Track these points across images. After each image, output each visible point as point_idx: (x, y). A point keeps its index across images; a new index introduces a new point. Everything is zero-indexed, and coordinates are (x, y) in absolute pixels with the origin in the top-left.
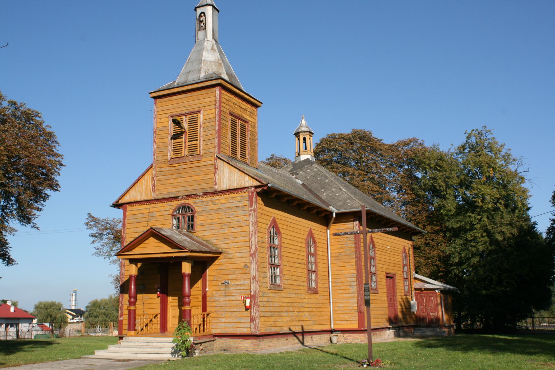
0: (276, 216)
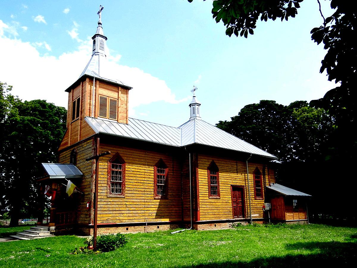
0: (119, 152)
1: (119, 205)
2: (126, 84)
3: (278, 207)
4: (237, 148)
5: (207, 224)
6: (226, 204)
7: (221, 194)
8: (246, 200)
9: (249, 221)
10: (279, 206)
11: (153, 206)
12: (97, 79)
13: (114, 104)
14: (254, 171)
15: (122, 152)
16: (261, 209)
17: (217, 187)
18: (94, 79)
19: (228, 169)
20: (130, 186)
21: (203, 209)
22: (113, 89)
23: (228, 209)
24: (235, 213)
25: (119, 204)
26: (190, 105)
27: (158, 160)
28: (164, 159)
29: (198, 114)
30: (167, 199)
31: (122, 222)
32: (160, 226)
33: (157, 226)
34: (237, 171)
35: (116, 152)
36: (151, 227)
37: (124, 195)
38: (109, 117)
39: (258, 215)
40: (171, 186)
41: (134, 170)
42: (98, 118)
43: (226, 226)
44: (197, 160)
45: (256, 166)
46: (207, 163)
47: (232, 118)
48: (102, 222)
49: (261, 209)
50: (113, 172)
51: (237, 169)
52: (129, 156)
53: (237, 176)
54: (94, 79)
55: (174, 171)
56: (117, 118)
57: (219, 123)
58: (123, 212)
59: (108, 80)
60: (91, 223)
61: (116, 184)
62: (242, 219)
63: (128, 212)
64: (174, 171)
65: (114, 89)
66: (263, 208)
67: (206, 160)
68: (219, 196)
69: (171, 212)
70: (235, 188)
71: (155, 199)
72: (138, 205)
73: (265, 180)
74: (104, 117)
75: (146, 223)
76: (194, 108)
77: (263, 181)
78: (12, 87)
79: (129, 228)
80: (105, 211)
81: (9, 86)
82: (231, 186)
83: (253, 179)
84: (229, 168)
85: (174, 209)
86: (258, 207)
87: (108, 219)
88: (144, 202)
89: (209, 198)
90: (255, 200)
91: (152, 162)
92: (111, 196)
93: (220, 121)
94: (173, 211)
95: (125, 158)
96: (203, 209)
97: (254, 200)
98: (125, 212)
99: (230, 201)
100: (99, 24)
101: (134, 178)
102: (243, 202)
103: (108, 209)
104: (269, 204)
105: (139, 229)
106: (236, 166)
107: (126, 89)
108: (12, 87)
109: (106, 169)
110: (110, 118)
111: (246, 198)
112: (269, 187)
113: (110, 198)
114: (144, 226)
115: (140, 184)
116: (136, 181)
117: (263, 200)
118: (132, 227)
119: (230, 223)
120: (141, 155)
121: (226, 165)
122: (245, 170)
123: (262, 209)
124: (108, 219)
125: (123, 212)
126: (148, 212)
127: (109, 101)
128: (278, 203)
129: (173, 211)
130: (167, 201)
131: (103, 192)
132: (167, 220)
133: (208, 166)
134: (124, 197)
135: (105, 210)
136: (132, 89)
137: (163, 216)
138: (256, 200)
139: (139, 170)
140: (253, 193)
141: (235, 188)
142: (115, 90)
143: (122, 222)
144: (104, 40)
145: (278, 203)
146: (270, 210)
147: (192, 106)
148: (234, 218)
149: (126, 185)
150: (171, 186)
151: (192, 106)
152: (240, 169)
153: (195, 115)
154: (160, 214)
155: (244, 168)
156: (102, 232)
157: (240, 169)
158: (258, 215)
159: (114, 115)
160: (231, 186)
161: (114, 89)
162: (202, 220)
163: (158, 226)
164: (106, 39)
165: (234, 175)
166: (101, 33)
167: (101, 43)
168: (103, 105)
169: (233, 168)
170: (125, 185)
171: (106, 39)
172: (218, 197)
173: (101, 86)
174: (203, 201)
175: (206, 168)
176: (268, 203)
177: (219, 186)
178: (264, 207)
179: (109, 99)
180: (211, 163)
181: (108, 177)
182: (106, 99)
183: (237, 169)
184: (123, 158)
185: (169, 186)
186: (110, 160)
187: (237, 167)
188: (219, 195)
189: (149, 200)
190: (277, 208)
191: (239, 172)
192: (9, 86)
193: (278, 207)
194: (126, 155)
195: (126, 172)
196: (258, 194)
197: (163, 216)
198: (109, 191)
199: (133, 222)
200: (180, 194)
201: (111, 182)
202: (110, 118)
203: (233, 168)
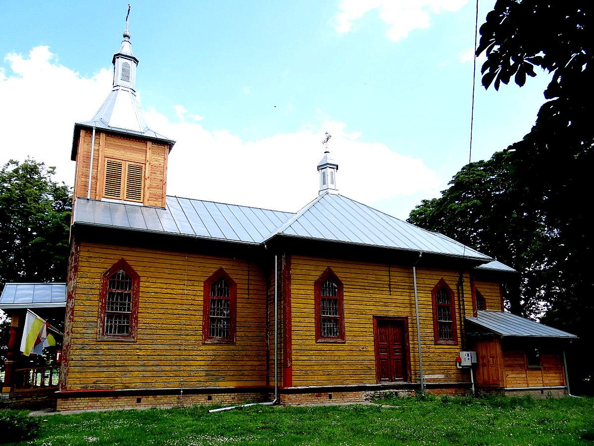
0: (126, 258)
1: (123, 356)
2: (162, 135)
3: (491, 359)
4: (428, 244)
5: (310, 394)
6: (359, 353)
7: (347, 334)
8: (411, 346)
9: (417, 388)
10: (493, 357)
11: (199, 358)
12: (99, 131)
13: (136, 173)
14: (434, 286)
15: (341, 271)
16: (452, 363)
17: (339, 322)
18: (94, 131)
19: (367, 284)
20: (148, 321)
21: (300, 363)
22: (135, 146)
23: (366, 363)
24: (383, 370)
25: (123, 354)
26: (320, 167)
27: (215, 270)
28: (226, 269)
29: (332, 183)
30: (234, 344)
31: (127, 387)
32: (214, 396)
33: (136, 397)
34: (390, 288)
35: (120, 257)
36: (193, 398)
37: (133, 337)
38: (126, 197)
39: (441, 376)
40: (243, 320)
41: (158, 290)
42: (103, 199)
43: (361, 399)
44: (288, 267)
45: (218, 266)
46: (314, 273)
47: (443, 192)
48: (84, 387)
49: (452, 363)
50: (112, 295)
51: (390, 285)
52: (149, 265)
53: (390, 297)
54: (94, 131)
55: (251, 292)
56: (142, 199)
57: (422, 204)
58: (131, 369)
59: (140, 134)
60: (60, 389)
61: (119, 316)
62: (401, 383)
63: (141, 369)
64: (251, 292)
65: (137, 147)
66: (456, 362)
67: (312, 268)
68: (343, 339)
69: (240, 368)
70: (381, 322)
71: (204, 344)
72: (164, 355)
73: (464, 305)
74: (116, 198)
75: (180, 390)
76: (324, 173)
77: (457, 307)
78: (54, 168)
79: (144, 399)
80: (90, 366)
81: (51, 168)
82: (375, 317)
83: (431, 303)
84: (370, 281)
85: (250, 363)
86: (444, 359)
87: (98, 381)
88: (180, 350)
89: (316, 343)
90: (435, 345)
91: (199, 274)
92: (105, 338)
93: (424, 201)
94: (246, 368)
95: (140, 269)
96: (300, 363)
97: (433, 346)
98: (136, 369)
99: (372, 348)
100: (125, 36)
101: (159, 306)
102: (405, 351)
103: (99, 364)
104: (469, 353)
105: (166, 401)
106: (387, 279)
107: (168, 144)
108: (54, 168)
109: (96, 291)
110: (127, 199)
111: (411, 342)
112: (474, 320)
113: (105, 343)
114: (177, 396)
115: (172, 316)
116: (162, 311)
117: (457, 345)
118: (151, 398)
119: (367, 393)
120: (174, 262)
121: (364, 276)
122: (411, 285)
123: (454, 363)
124: (98, 381)
125: (131, 369)
126: (188, 368)
127: (127, 169)
128: (490, 352)
129: (246, 368)
130: (232, 347)
131: (89, 331)
132: (231, 385)
133: (316, 278)
134: (133, 340)
135: (91, 365)
136: (176, 143)
137: (223, 377)
138: (437, 347)
139: (168, 291)
140: (431, 330)
141: (381, 322)
142: (140, 148)
143: (127, 387)
144: (131, 63)
145: (490, 352)
146: (474, 366)
147: (321, 169)
148: (379, 380)
149: (139, 319)
150: (243, 320)
151: (321, 169)
152: (397, 284)
153: (328, 186)
154: (216, 374)
155: (407, 281)
156: (84, 406)
157: (397, 284)
158: (441, 376)
159: (134, 192)
160: (375, 317)
161: (137, 147)
162: (297, 384)
163: (139, 397)
164: (136, 61)
165: (382, 296)
166: (127, 50)
167: (123, 70)
168: (113, 177)
169: (380, 282)
170: (136, 318)
171: (136, 61)
172: (339, 340)
173: (108, 142)
174: (300, 348)
175: (312, 283)
176: (468, 352)
177: (342, 318)
178: (459, 360)
179: (106, 161)
180: (323, 274)
181: (101, 304)
182: (120, 165)
183: (390, 285)
184: (135, 268)
185: (238, 319)
186: (107, 273)
187: (390, 279)
188: (342, 336)
189: (190, 346)
190: (489, 361)
191: (394, 290)
192: (51, 168)
193: (491, 359)
194: (141, 264)
195: (141, 294)
196: (443, 332)
197: (223, 377)
198: (101, 329)
199: (154, 387)
200: (263, 334)
201: (105, 312)
202: (127, 199)
203: (380, 282)
